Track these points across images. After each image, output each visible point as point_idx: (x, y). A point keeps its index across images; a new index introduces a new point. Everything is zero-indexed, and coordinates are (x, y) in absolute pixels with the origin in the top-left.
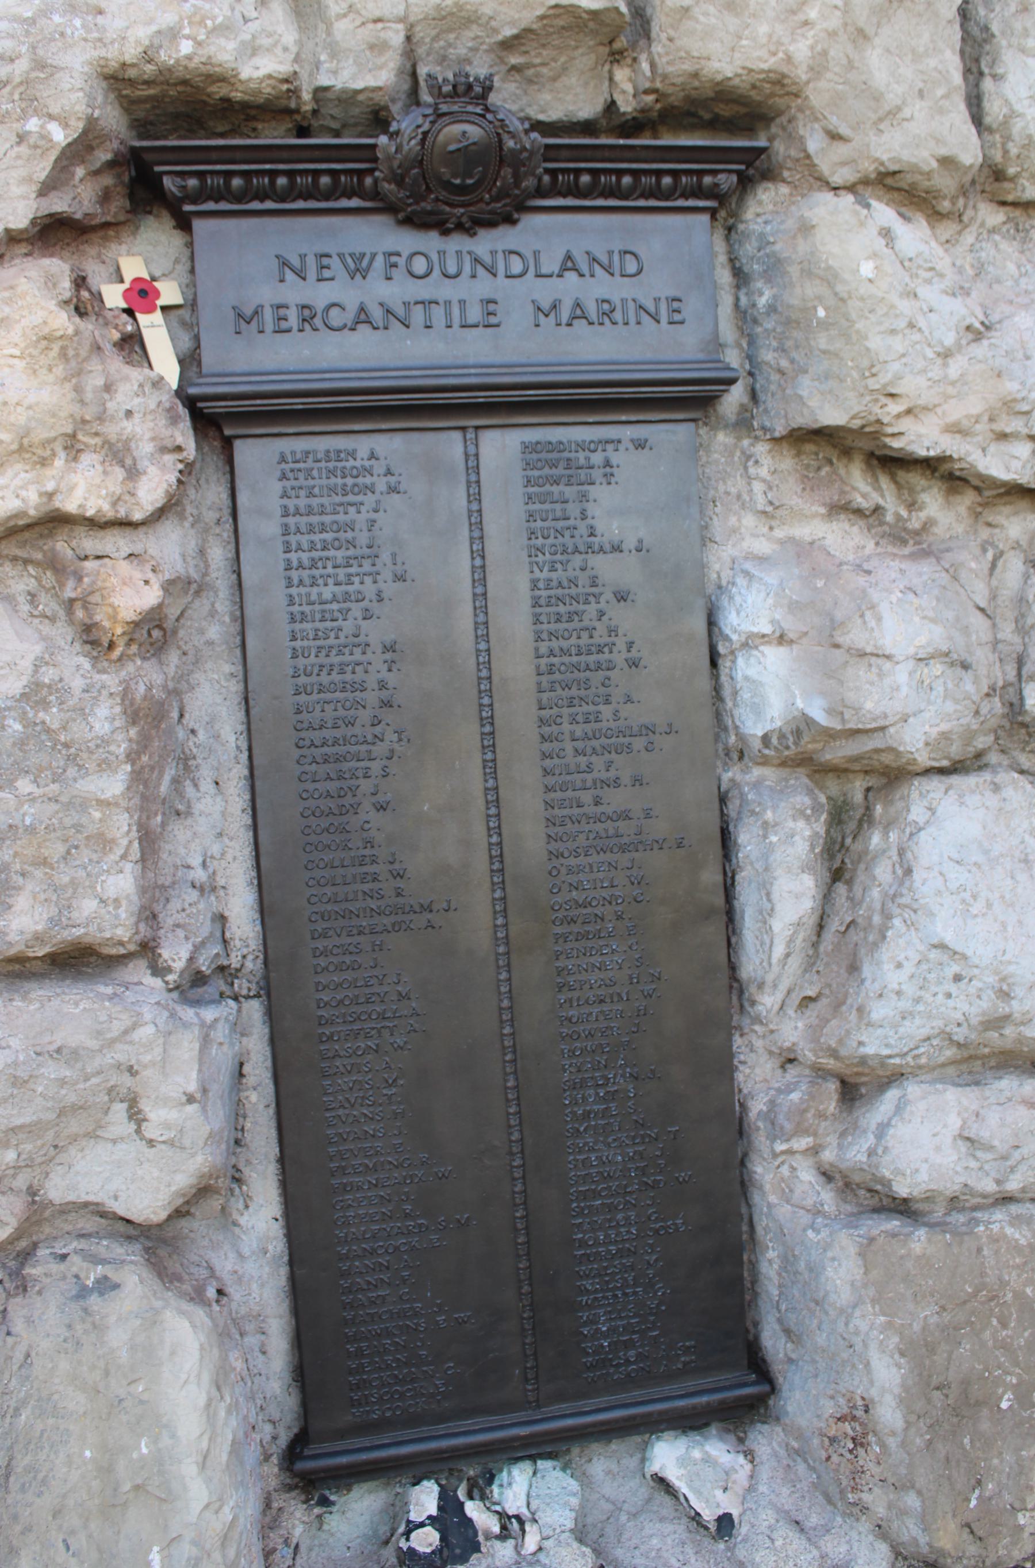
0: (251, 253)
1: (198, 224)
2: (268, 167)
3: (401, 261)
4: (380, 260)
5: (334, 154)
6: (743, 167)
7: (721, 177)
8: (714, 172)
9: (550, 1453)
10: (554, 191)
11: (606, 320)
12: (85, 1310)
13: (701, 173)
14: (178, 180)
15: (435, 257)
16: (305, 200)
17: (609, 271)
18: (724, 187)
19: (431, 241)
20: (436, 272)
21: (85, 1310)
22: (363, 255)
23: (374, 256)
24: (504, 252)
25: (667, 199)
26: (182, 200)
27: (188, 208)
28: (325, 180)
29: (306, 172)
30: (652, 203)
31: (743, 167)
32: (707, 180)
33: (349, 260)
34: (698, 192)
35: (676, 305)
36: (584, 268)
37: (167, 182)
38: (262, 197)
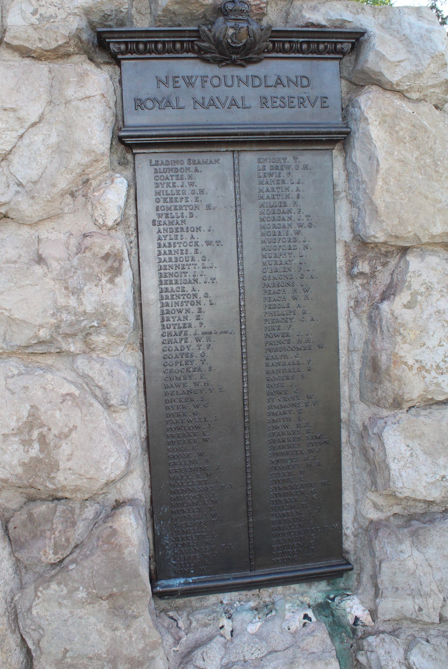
0: (144, 74)
1: (123, 62)
2: (316, 40)
3: (209, 80)
4: (199, 79)
5: (317, 35)
6: (354, 41)
7: (345, 44)
8: (342, 43)
9: (425, 624)
10: (274, 50)
11: (302, 106)
12: (398, 649)
13: (336, 43)
14: (117, 46)
15: (222, 78)
16: (169, 53)
17: (296, 84)
18: (345, 49)
19: (230, 71)
20: (263, 85)
21: (398, 649)
22: (192, 77)
23: (197, 77)
24: (252, 76)
25: (321, 54)
26: (118, 53)
27: (120, 57)
28: (305, 46)
29: (280, 41)
30: (315, 56)
31: (354, 41)
32: (339, 46)
33: (187, 79)
34: (335, 51)
35: (324, 99)
36: (285, 83)
37: (111, 46)
38: (150, 52)
